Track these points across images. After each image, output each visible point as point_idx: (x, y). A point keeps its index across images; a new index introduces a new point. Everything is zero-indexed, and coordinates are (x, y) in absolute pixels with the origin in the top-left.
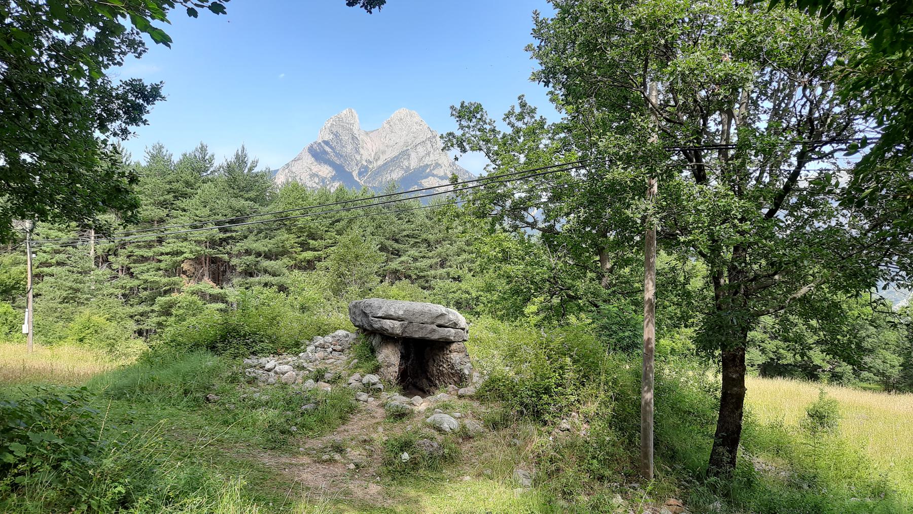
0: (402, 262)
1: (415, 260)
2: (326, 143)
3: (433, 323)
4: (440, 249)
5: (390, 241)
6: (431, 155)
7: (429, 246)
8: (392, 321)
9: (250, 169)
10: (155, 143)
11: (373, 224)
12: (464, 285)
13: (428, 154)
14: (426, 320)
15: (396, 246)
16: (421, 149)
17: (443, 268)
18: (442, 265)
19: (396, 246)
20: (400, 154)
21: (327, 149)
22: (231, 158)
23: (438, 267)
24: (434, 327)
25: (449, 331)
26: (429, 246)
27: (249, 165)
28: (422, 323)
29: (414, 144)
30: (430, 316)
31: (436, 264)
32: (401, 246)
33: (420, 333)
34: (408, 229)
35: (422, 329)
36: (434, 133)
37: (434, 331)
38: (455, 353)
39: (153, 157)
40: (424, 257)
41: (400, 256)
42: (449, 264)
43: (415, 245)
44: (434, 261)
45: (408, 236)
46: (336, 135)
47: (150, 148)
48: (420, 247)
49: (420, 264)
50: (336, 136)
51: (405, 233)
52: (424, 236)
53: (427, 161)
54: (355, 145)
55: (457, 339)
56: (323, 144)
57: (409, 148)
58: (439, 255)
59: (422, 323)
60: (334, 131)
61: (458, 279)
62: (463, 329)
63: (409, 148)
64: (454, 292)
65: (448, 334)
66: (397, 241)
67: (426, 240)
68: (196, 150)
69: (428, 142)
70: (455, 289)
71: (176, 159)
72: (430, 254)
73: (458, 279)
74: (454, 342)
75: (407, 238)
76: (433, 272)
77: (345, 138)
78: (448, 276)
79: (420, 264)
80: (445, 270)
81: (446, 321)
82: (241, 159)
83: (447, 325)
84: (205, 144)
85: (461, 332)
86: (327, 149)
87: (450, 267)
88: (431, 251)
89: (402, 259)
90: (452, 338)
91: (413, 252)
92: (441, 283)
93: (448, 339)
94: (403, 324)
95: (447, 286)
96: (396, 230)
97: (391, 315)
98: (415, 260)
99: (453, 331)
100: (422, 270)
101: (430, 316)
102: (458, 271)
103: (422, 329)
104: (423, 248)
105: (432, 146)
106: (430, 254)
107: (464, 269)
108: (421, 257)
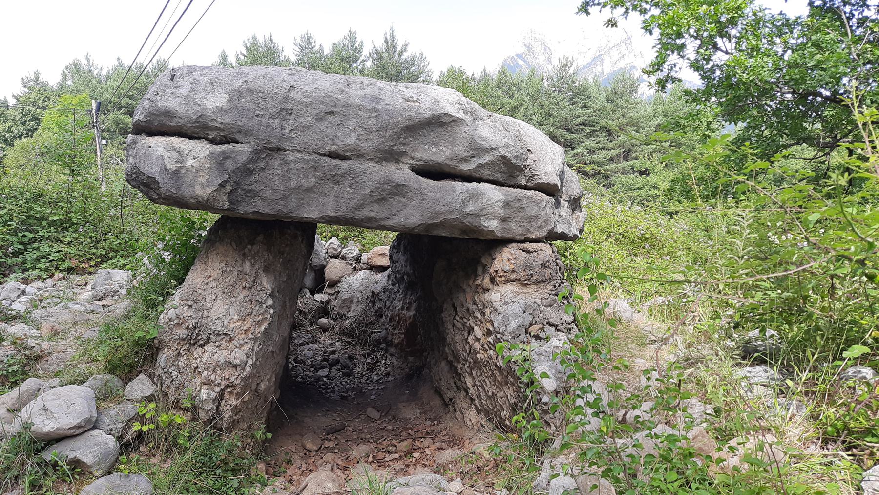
0: (575, 155)
1: (592, 152)
2: (519, 56)
3: (391, 156)
4: (623, 138)
5: (560, 131)
6: (626, 57)
7: (609, 135)
8: (176, 141)
9: (400, 55)
10: (304, 33)
11: (540, 111)
12: (652, 179)
13: (623, 57)
14: (351, 140)
15: (569, 136)
16: (615, 54)
17: (627, 161)
18: (626, 159)
19: (569, 136)
20: (593, 60)
21: (520, 62)
22: (380, 44)
23: (622, 160)
24: (402, 173)
25: (474, 196)
26: (609, 135)
27: (398, 50)
28: (332, 155)
29: (608, 48)
30: (372, 123)
31: (618, 156)
32: (574, 136)
33: (330, 202)
34: (582, 115)
35: (336, 179)
36: (630, 34)
37: (398, 190)
38: (511, 288)
39: (302, 49)
40: (603, 148)
41: (573, 149)
42: (634, 155)
43: (592, 134)
44: (614, 153)
45: (583, 124)
46: (529, 47)
47: (299, 41)
48: (598, 136)
49: (600, 156)
50: (529, 48)
51: (579, 120)
52: (603, 122)
53: (621, 64)
54: (547, 56)
55: (515, 229)
56: (516, 57)
57: (602, 52)
58: (622, 145)
59: (332, 155)
60: (527, 43)
61: (644, 173)
62: (550, 190)
63: (602, 52)
64: (639, 188)
65: (470, 208)
66: (569, 130)
67: (606, 128)
68: (345, 38)
69: (623, 44)
70: (641, 185)
71: (327, 50)
72: (611, 145)
73: (644, 173)
74: (505, 242)
75: (582, 127)
76: (613, 166)
77: (538, 48)
78: (633, 168)
79: (600, 156)
80: (629, 163)
81: (461, 149)
82: (391, 45)
83: (465, 167)
84: (353, 31)
85: (537, 203)
86: (520, 62)
87: (636, 158)
88: (611, 141)
89: (575, 151)
90: (492, 225)
91: (590, 143)
92: (623, 179)
93: (477, 230)
94: (225, 156)
95: (630, 181)
96: (568, 116)
97: (168, 114)
98: (592, 152)
99: (493, 194)
100: (600, 164)
101: (372, 123)
102: (646, 162)
103: (336, 179)
104: (602, 138)
105: (627, 48)
106: (611, 145)
107: (653, 160)
108: (599, 149)
